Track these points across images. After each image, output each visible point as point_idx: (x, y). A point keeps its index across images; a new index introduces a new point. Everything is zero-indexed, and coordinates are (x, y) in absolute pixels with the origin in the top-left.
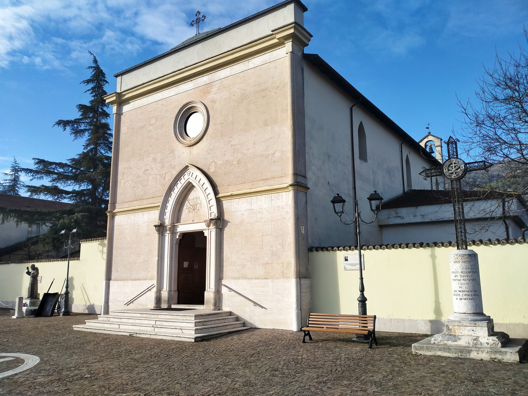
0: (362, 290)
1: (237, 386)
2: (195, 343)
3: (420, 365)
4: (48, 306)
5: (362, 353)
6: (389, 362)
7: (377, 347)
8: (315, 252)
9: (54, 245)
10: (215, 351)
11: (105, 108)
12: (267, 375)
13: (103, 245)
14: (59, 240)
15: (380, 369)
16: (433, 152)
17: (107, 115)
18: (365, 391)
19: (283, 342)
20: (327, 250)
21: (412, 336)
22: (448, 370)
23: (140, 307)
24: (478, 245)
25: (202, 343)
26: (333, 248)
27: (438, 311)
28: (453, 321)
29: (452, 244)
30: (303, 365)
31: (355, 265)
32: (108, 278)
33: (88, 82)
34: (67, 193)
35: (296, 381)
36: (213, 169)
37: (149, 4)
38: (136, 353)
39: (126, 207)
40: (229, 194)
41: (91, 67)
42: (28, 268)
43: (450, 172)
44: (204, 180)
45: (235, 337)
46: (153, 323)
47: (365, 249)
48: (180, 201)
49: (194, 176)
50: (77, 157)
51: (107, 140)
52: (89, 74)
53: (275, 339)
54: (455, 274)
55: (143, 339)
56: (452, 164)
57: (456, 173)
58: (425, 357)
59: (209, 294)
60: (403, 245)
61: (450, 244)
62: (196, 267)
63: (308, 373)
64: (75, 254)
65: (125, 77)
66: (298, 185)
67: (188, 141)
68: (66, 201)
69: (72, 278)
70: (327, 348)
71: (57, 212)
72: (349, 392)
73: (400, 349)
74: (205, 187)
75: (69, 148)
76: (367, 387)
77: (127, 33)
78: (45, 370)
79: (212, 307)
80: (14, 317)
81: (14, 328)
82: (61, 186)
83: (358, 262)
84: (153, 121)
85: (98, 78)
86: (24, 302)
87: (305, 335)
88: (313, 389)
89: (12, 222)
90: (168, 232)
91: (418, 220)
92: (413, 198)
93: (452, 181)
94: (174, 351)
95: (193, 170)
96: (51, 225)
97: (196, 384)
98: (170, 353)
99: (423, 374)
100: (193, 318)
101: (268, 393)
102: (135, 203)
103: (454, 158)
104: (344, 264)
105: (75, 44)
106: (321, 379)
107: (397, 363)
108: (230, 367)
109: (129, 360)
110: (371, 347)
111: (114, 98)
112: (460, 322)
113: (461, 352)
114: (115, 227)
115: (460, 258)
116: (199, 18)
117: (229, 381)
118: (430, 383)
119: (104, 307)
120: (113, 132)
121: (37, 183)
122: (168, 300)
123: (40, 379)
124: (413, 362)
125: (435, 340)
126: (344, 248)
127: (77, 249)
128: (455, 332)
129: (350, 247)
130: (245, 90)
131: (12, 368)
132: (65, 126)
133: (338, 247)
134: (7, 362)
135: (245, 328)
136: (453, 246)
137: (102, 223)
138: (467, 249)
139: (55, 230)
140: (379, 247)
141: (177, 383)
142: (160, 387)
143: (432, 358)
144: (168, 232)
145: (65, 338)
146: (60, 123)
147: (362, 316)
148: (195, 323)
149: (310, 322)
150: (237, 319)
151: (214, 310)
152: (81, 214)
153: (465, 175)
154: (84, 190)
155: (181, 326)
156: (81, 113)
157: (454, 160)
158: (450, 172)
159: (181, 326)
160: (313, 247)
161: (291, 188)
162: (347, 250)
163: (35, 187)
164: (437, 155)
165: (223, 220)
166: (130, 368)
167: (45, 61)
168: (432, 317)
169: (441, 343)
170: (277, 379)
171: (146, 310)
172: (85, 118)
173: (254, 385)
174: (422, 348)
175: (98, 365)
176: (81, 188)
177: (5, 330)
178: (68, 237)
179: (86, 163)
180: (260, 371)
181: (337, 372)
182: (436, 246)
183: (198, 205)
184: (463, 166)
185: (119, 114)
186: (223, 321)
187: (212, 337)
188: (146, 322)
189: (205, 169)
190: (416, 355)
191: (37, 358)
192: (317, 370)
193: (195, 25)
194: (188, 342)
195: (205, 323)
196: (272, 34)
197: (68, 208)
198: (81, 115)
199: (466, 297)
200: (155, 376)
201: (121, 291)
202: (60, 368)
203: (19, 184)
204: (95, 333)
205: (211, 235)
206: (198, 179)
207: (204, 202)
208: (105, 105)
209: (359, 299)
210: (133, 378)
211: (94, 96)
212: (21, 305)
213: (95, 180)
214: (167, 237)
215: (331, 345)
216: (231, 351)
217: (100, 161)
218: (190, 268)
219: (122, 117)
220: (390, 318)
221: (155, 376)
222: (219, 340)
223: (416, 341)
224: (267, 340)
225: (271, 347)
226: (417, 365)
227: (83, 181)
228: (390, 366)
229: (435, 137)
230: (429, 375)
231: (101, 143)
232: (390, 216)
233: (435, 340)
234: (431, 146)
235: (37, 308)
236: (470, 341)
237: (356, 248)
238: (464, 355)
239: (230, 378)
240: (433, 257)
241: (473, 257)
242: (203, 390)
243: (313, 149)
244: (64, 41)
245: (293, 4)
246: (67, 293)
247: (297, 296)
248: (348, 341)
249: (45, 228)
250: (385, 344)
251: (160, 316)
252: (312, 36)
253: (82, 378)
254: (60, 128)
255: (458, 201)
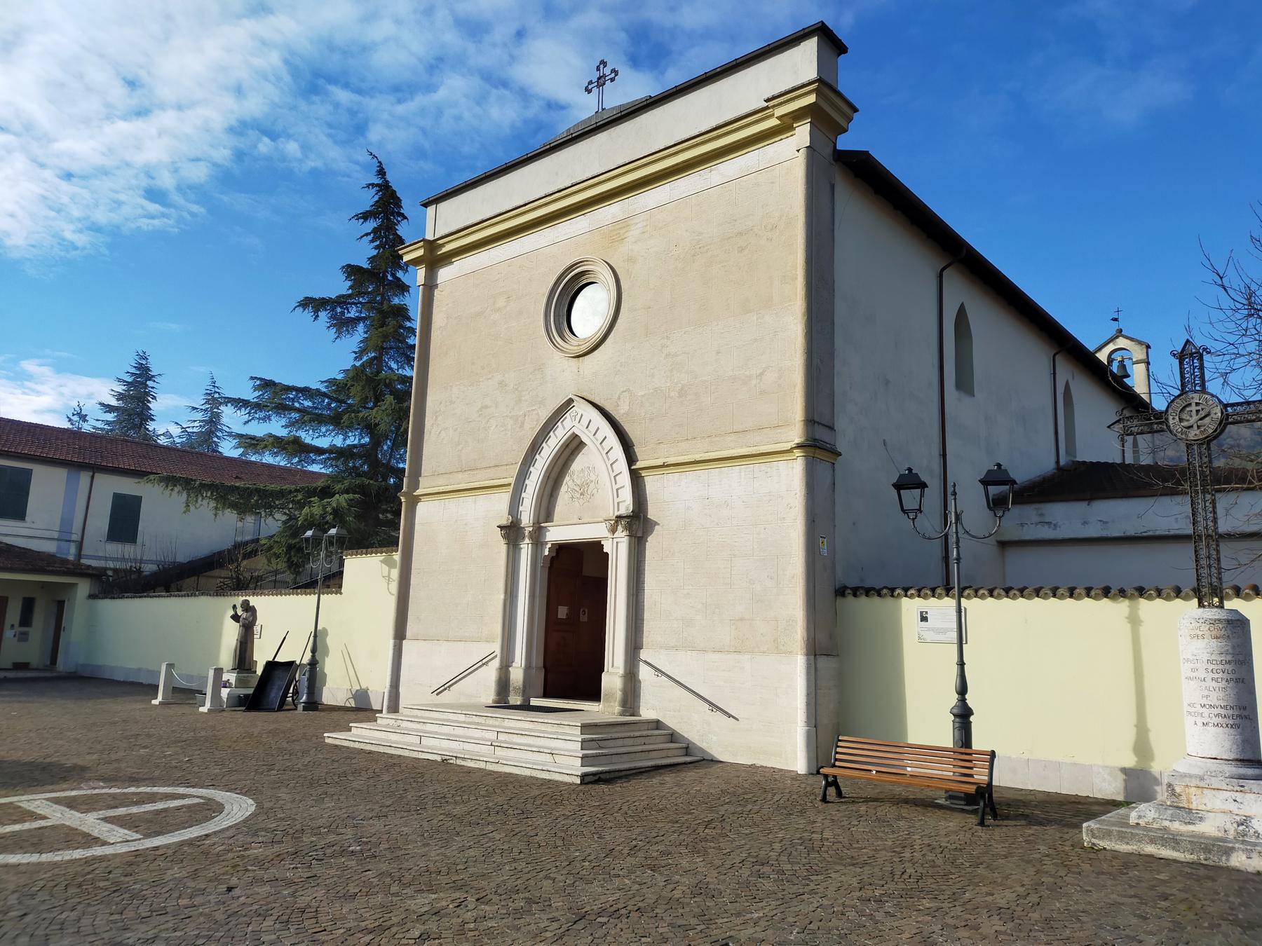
0: (962, 690)
1: (677, 894)
2: (582, 787)
3: (1103, 873)
4: (274, 689)
5: (961, 836)
6: (1028, 862)
7: (997, 822)
8: (850, 599)
9: (289, 559)
10: (625, 808)
11: (400, 274)
12: (745, 872)
13: (389, 563)
14: (300, 549)
15: (1007, 878)
16: (1128, 376)
17: (403, 288)
18: (976, 928)
19: (776, 798)
20: (879, 595)
21: (1079, 803)
22: (1174, 891)
23: (463, 700)
24: (1247, 598)
25: (596, 786)
26: (892, 590)
27: (1142, 747)
28: (1185, 776)
29: (1182, 594)
30: (825, 855)
31: (944, 631)
32: (400, 634)
33: (365, 216)
34: (320, 451)
35: (812, 892)
36: (626, 408)
37: (550, 13)
38: (456, 803)
39: (441, 484)
40: (660, 462)
41: (373, 185)
42: (234, 607)
43: (1185, 424)
44: (607, 430)
45: (667, 779)
46: (493, 736)
47: (968, 597)
48: (554, 475)
49: (585, 422)
50: (340, 377)
51: (403, 342)
52: (369, 199)
53: (757, 786)
54: (1192, 666)
55: (470, 771)
56: (1190, 405)
57: (1199, 427)
58: (1115, 854)
59: (612, 679)
60: (1060, 591)
61: (1178, 593)
62: (584, 618)
63: (837, 875)
64: (333, 581)
65: (444, 206)
66: (815, 446)
67: (574, 346)
68: (315, 468)
69: (325, 631)
70: (878, 819)
71: (297, 491)
72: (937, 928)
73: (1051, 832)
74: (607, 445)
75: (325, 357)
76: (979, 920)
77: (495, 80)
78: (266, 830)
79: (617, 709)
80: (204, 709)
81: (203, 733)
82: (307, 437)
83: (954, 625)
84: (501, 302)
85: (386, 208)
86: (225, 677)
87: (828, 784)
88: (851, 914)
89: (205, 507)
90: (527, 541)
91: (1093, 531)
92: (1080, 481)
93: (1188, 446)
94: (538, 802)
95: (581, 408)
96: (284, 518)
97: (589, 882)
98: (529, 806)
99: (1113, 896)
100: (578, 731)
101: (749, 916)
102: (460, 476)
103: (1196, 392)
104: (922, 631)
105: (380, 106)
106: (870, 893)
107: (1049, 866)
108: (661, 848)
109: (442, 817)
110: (982, 823)
111: (421, 252)
112: (1202, 779)
113: (1207, 850)
114: (417, 527)
115: (1205, 628)
116: (604, 76)
117: (660, 880)
118: (1134, 921)
119: (390, 696)
120: (417, 325)
121: (258, 429)
122: (524, 686)
123: (257, 851)
124: (1086, 867)
125: (1140, 817)
126: (919, 591)
127: (335, 569)
128: (1189, 801)
129: (933, 590)
130: (701, 233)
131: (199, 822)
132: (316, 311)
133: (906, 590)
134: (189, 808)
135: (688, 759)
136: (1186, 598)
137: (389, 516)
138: (1222, 607)
139: (293, 529)
140: (1003, 593)
141: (547, 877)
142: (510, 885)
143: (1132, 858)
144: (527, 541)
145: (309, 759)
146: (306, 303)
147: (963, 750)
148: (583, 741)
149: (838, 756)
150: (673, 737)
151: (622, 714)
152: (351, 496)
153: (1222, 431)
154: (355, 446)
155: (550, 747)
156: (349, 283)
157: (1196, 396)
158: (1185, 424)
159: (550, 747)
160: (846, 588)
161: (798, 453)
162: (925, 597)
163: (253, 438)
164: (1138, 381)
165: (646, 518)
166: (445, 836)
167: (306, 148)
168: (1130, 761)
169: (1155, 826)
170: (767, 885)
171: (475, 707)
172: (360, 294)
173: (716, 893)
174: (1107, 834)
175: (378, 825)
176: (348, 442)
177: (185, 736)
178: (320, 543)
179: (359, 388)
180: (728, 864)
181: (906, 876)
182: (1141, 596)
183: (592, 486)
184: (1218, 410)
185: (430, 286)
186: (642, 740)
187: (617, 774)
188: (477, 734)
189: (608, 408)
190: (1093, 849)
191: (251, 802)
192: (858, 870)
193: (595, 90)
194: (566, 784)
195: (601, 743)
196: (767, 108)
197: (320, 483)
198: (350, 288)
199: (1220, 720)
200: (497, 858)
201: (427, 663)
202: (299, 827)
203: (221, 430)
204: (370, 752)
205: (617, 549)
206: (592, 428)
207: (605, 479)
208: (401, 268)
209: (955, 711)
210: (452, 860)
211: (376, 248)
212: (219, 684)
213: (376, 425)
214: (526, 549)
215: (886, 811)
216: (661, 810)
217: (387, 386)
218: (572, 623)
219: (436, 292)
220: (1027, 756)
221: (497, 858)
222: (633, 782)
223: (1091, 816)
224: (741, 791)
225: (750, 807)
226: (1098, 874)
227: (350, 427)
228: (1031, 871)
229: (1132, 339)
230: (1130, 900)
231: (391, 348)
232: (1025, 521)
233: (1140, 817)
234: (1122, 361)
235: (251, 691)
236: (1228, 826)
237: (948, 591)
238: (1214, 859)
239: (661, 874)
240: (1134, 621)
241: (1238, 629)
242: (603, 899)
243: (850, 367)
244: (356, 98)
245: (816, 39)
246: (313, 663)
247: (808, 695)
248: (928, 804)
249: (272, 524)
250: (1016, 817)
251: (507, 723)
252: (856, 110)
253: (343, 852)
254: (308, 315)
255: (1204, 492)
